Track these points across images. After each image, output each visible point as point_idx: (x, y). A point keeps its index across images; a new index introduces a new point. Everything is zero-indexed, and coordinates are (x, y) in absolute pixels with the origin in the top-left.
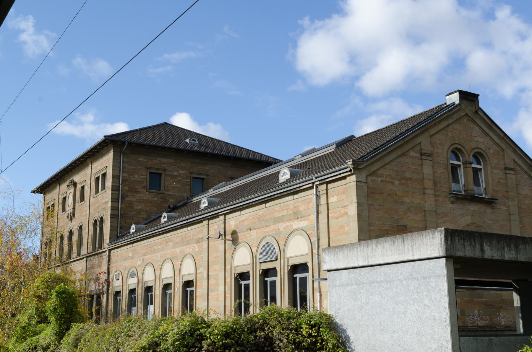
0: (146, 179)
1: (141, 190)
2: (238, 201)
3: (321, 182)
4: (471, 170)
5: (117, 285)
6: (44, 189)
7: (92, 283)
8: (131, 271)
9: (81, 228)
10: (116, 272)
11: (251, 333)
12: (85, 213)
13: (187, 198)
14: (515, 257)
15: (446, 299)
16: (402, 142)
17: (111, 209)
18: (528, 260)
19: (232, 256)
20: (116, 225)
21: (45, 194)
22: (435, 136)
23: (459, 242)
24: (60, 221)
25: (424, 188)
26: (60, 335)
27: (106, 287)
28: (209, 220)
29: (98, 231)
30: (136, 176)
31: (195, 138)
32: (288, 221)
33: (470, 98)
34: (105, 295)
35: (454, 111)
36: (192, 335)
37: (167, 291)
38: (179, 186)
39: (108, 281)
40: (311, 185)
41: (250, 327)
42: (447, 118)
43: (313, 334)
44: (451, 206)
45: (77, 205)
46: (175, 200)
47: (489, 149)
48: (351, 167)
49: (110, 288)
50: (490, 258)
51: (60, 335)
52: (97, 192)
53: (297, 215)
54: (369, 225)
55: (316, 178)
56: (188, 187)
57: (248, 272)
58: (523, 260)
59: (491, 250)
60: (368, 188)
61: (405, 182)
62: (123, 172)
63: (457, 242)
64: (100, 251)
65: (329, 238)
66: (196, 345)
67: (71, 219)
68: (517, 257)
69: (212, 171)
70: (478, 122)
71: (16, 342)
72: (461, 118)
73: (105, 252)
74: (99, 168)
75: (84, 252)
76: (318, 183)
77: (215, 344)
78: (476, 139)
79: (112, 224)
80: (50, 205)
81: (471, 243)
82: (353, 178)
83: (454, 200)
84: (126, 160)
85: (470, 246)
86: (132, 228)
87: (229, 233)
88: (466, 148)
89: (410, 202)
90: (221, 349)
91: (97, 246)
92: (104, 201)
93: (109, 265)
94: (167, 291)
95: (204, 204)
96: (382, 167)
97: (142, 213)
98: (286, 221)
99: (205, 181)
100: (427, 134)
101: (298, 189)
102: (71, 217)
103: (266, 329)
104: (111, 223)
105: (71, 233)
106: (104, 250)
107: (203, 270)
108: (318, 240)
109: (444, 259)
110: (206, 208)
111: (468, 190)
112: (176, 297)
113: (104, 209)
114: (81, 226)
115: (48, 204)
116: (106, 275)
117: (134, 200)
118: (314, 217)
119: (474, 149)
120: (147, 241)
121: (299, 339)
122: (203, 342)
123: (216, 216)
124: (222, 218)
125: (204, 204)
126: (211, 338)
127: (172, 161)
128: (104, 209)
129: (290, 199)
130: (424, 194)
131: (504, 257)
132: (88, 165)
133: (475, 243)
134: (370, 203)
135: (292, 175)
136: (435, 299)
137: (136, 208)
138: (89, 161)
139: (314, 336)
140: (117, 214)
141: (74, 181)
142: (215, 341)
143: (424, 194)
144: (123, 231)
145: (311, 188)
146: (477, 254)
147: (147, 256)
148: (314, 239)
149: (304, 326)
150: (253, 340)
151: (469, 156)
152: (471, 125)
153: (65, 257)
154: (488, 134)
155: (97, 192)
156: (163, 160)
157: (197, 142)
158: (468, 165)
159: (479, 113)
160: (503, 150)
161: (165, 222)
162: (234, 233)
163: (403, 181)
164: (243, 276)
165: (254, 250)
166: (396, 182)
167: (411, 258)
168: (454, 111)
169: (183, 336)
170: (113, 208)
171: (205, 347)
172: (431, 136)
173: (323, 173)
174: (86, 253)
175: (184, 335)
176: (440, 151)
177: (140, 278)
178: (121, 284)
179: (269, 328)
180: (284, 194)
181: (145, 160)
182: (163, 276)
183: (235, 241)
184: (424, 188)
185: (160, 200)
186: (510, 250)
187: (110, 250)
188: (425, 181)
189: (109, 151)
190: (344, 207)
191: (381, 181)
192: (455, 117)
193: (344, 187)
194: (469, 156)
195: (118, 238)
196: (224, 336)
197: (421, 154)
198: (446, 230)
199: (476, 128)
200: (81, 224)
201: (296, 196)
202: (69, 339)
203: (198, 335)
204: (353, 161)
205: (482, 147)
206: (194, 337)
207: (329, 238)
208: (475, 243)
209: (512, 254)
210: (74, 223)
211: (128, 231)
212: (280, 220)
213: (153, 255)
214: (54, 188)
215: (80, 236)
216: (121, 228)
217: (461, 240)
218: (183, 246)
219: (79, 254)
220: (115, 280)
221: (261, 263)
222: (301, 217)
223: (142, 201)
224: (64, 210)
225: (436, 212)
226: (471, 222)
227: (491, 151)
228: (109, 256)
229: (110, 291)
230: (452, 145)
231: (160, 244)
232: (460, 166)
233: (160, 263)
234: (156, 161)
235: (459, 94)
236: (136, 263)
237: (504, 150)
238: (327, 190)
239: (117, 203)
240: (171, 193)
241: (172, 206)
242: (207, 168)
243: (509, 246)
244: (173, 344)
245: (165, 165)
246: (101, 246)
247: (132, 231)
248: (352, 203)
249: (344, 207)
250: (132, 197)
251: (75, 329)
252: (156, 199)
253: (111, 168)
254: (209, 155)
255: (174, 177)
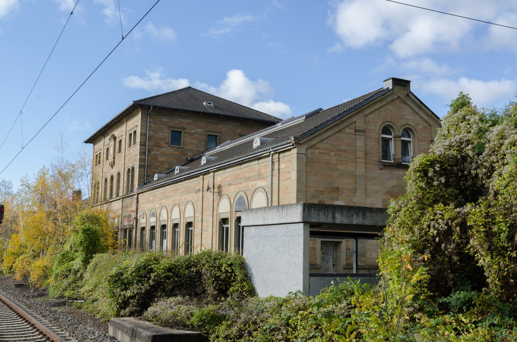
0: (169, 136)
1: (164, 145)
2: (222, 162)
3: (275, 152)
4: (400, 143)
5: (142, 222)
6: (93, 140)
7: (126, 219)
8: (152, 212)
9: (119, 174)
10: (142, 211)
11: (187, 269)
12: (121, 163)
13: (203, 152)
14: (363, 222)
15: (302, 252)
16: (338, 122)
17: (139, 161)
18: (373, 224)
19: (218, 205)
20: (143, 173)
21: (94, 144)
22: (369, 116)
23: (314, 212)
24: (105, 167)
25: (356, 158)
26: (86, 262)
27: (135, 223)
28: (203, 175)
29: (130, 178)
30: (160, 134)
31: (211, 101)
32: (254, 180)
33: (402, 83)
34: (134, 229)
35: (387, 95)
36: (145, 269)
37: (176, 229)
38: (196, 142)
39: (136, 219)
40: (268, 154)
41: (188, 265)
42: (381, 100)
43: (229, 271)
44: (380, 172)
45: (116, 155)
46: (192, 154)
47: (418, 125)
48: (294, 142)
49: (138, 224)
50: (340, 223)
51: (86, 262)
52: (130, 146)
53: (260, 177)
54: (307, 187)
55: (272, 148)
56: (203, 143)
57: (228, 218)
58: (369, 224)
59: (342, 217)
60: (307, 158)
61: (340, 153)
62: (149, 130)
63: (313, 212)
64: (111, 200)
65: (279, 195)
66: (147, 276)
67: (112, 167)
68: (364, 222)
69: (224, 129)
70: (409, 103)
71: (58, 265)
72: (394, 100)
73: (135, 195)
74: (132, 126)
75: (121, 194)
76: (273, 152)
77: (160, 276)
78: (406, 117)
79: (140, 173)
80: (98, 153)
81: (325, 213)
82: (295, 151)
83: (382, 167)
84: (151, 120)
85: (324, 215)
86: (155, 177)
87: (216, 186)
88: (396, 125)
89: (343, 168)
90: (163, 279)
91: (130, 190)
92: (135, 154)
93: (137, 206)
94: (176, 229)
95: (257, 143)
96: (321, 141)
97: (165, 164)
98: (253, 180)
99: (218, 138)
100: (362, 114)
101: (260, 156)
102: (112, 165)
103: (198, 266)
104: (139, 172)
105: (112, 177)
106: (134, 194)
107: (198, 215)
108: (272, 196)
109: (302, 224)
110: (205, 165)
111: (396, 159)
112: (181, 234)
113: (135, 160)
114: (119, 173)
115: (97, 152)
116: (135, 213)
117: (158, 153)
118: (270, 178)
119: (403, 125)
120: (163, 188)
121: (218, 273)
122: (151, 274)
123: (208, 173)
124: (212, 174)
125: (257, 143)
126: (158, 271)
127: (191, 121)
128: (135, 160)
129: (256, 163)
130: (356, 162)
131: (352, 222)
132: (124, 123)
133: (328, 213)
134: (308, 170)
135: (262, 143)
136: (297, 251)
137: (160, 160)
138: (124, 120)
139: (230, 272)
140: (144, 165)
141: (114, 135)
142: (160, 273)
143: (356, 162)
144: (149, 178)
145: (269, 156)
146: (330, 220)
147: (163, 201)
148: (269, 196)
149: (224, 265)
150: (187, 274)
151: (399, 132)
152: (403, 106)
153: (108, 197)
154: (417, 113)
155: (130, 146)
156: (183, 120)
157: (212, 105)
158: (397, 139)
159: (410, 95)
160: (430, 125)
161: (177, 174)
162: (220, 187)
163: (338, 153)
164: (224, 221)
165: (232, 201)
166: (332, 154)
167: (286, 222)
168: (387, 95)
169: (138, 269)
170: (140, 160)
171: (152, 277)
172: (365, 116)
173: (276, 146)
174: (122, 195)
175: (139, 268)
176: (373, 128)
177: (158, 218)
178: (145, 222)
179: (200, 266)
180: (252, 159)
181: (168, 120)
182: (173, 218)
183: (220, 193)
184: (356, 158)
185: (180, 153)
186: (358, 217)
187: (138, 194)
188: (357, 152)
189: (138, 113)
190: (290, 172)
191: (319, 152)
192: (389, 99)
193: (290, 157)
194: (399, 132)
195: (145, 184)
196: (167, 270)
197: (356, 131)
198: (304, 204)
199: (407, 108)
200: (119, 171)
201: (260, 161)
202: (90, 266)
203: (149, 269)
204: (294, 138)
205: (412, 123)
206: (146, 270)
207: (279, 195)
208: (328, 213)
209: (360, 220)
210: (114, 170)
211: (152, 179)
212: (248, 179)
213: (166, 200)
214: (101, 140)
215: (118, 180)
216: (147, 176)
217: (317, 210)
218: (186, 194)
219: (117, 195)
220: (141, 218)
221: (236, 211)
222: (262, 178)
223: (165, 154)
224: (107, 159)
225: (365, 176)
226: (396, 185)
227: (420, 127)
228: (137, 198)
229: (138, 226)
230: (384, 122)
231: (172, 191)
232: (391, 139)
233: (171, 207)
234: (177, 121)
235: (393, 80)
236: (156, 206)
237: (431, 126)
238: (279, 158)
239: (144, 156)
240: (189, 148)
241: (189, 159)
242: (219, 127)
243: (357, 214)
244: (131, 275)
245: (185, 125)
246: (132, 191)
247: (155, 179)
248: (294, 170)
249: (290, 172)
250: (157, 151)
251: (97, 257)
252: (176, 153)
253: (140, 127)
254: (222, 116)
255: (192, 134)
